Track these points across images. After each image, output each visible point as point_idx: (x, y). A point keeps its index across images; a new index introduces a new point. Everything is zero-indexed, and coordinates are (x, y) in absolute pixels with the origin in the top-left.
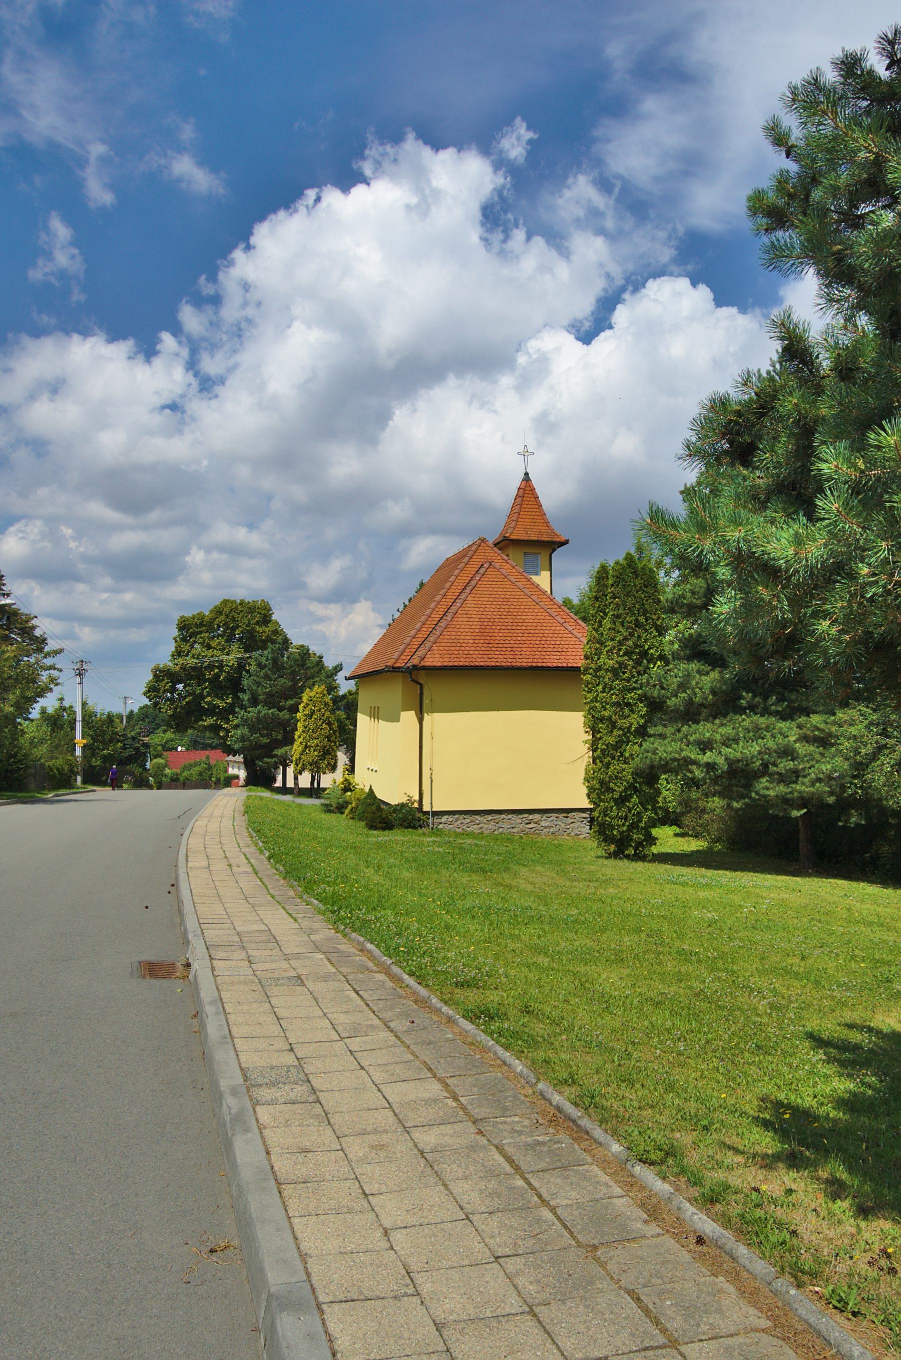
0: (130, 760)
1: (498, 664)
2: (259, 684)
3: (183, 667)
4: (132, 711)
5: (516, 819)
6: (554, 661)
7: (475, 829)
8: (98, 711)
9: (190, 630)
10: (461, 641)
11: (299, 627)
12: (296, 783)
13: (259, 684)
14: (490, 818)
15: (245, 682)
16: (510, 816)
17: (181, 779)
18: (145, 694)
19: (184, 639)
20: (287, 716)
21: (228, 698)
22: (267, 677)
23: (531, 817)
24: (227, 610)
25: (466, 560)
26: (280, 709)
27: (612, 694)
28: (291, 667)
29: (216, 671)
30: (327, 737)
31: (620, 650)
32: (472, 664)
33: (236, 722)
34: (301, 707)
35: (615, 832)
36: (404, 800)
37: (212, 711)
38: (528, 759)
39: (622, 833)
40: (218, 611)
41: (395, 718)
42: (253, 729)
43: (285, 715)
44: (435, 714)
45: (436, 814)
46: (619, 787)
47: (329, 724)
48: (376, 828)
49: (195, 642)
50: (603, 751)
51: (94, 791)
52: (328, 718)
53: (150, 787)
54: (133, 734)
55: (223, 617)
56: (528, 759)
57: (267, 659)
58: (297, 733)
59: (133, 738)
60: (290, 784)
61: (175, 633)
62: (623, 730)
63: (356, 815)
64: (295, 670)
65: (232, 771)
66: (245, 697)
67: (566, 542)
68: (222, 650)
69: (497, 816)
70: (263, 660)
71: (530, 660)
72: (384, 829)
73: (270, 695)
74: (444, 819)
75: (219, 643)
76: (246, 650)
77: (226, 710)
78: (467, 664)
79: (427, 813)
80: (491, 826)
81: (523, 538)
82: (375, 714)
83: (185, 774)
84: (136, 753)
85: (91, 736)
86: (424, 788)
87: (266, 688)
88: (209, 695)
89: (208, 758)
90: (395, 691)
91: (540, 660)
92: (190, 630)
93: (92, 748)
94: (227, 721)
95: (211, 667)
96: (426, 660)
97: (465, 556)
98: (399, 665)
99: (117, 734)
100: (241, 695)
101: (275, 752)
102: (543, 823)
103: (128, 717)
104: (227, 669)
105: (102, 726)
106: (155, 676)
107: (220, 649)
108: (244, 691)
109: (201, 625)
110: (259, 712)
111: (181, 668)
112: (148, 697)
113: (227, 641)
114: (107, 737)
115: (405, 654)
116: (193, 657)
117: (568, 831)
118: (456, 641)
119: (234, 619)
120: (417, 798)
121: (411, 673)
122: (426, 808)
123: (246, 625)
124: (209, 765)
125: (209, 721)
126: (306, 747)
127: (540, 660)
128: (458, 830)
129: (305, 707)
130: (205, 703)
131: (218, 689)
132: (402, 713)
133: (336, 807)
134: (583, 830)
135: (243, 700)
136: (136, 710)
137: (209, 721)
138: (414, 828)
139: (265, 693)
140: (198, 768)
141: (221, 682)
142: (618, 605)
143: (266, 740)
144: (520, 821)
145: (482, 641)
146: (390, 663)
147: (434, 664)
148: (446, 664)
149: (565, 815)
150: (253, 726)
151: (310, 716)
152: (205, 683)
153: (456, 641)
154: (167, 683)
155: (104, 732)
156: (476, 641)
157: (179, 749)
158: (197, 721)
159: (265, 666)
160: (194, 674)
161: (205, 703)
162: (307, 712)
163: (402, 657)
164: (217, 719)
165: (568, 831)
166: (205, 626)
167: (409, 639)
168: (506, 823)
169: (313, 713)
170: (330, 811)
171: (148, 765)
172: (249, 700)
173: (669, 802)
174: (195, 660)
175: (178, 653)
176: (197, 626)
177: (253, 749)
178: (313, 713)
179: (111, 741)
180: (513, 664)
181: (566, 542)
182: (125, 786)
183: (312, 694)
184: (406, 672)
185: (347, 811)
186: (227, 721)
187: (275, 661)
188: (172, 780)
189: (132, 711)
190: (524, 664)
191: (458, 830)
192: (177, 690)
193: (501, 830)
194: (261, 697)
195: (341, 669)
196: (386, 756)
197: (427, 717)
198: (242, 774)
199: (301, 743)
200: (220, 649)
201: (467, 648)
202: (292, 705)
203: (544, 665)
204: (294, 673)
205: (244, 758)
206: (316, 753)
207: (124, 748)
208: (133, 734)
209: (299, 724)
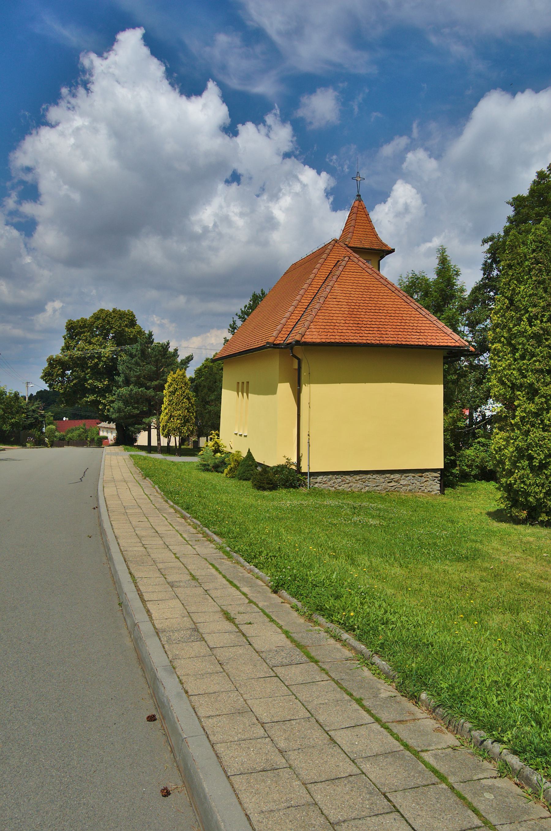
0: (31, 426)
1: (369, 342)
2: (131, 369)
3: (71, 358)
4: (32, 395)
5: (380, 478)
6: (414, 340)
7: (345, 487)
8: (8, 391)
9: (74, 330)
10: (335, 321)
11: (158, 328)
12: (159, 444)
13: (131, 369)
14: (358, 478)
15: (120, 368)
16: (374, 476)
17: (67, 439)
18: (42, 378)
19: (71, 338)
20: (153, 394)
21: (105, 381)
22: (137, 364)
23: (392, 477)
24: (103, 315)
25: (324, 256)
26: (148, 388)
27: (535, 361)
28: (156, 356)
29: (96, 360)
30: (187, 409)
31: (543, 316)
32: (347, 341)
33: (111, 398)
34: (166, 386)
35: (531, 499)
36: (283, 462)
37: (93, 390)
38: (395, 425)
39: (538, 500)
40: (96, 317)
41: (273, 391)
42: (126, 403)
43: (151, 392)
44: (311, 385)
45: (313, 474)
46: (539, 454)
47: (188, 399)
48: (264, 489)
49: (80, 339)
50: (522, 418)
51: (4, 450)
52: (187, 394)
53: (45, 445)
54: (33, 408)
55: (100, 321)
56: (395, 425)
57: (137, 351)
58: (163, 406)
59: (34, 411)
60: (154, 443)
61: (65, 332)
62: (545, 397)
63: (232, 474)
64: (158, 359)
65: (102, 434)
66: (120, 379)
67: (393, 251)
68: (100, 345)
69: (364, 476)
70: (134, 351)
71: (396, 339)
72: (271, 489)
73: (138, 377)
74: (319, 479)
75: (98, 340)
76: (118, 345)
77: (103, 390)
78: (342, 341)
79: (305, 474)
80: (359, 485)
81: (358, 246)
82: (244, 388)
83: (69, 435)
84: (36, 421)
85: (2, 409)
86: (301, 452)
87: (136, 372)
88: (90, 378)
89: (84, 425)
90: (273, 365)
91: (403, 339)
92: (74, 330)
93: (3, 418)
94: (105, 397)
95: (92, 357)
96: (305, 336)
97: (323, 253)
98: (278, 342)
99: (21, 407)
100: (116, 378)
101: (144, 420)
102: (402, 482)
103: (29, 398)
104: (104, 359)
105: (10, 402)
106: (50, 364)
107: (98, 345)
108: (118, 375)
109: (84, 326)
110: (132, 390)
111: (70, 358)
112: (45, 380)
113: (103, 338)
114: (14, 410)
115: (282, 332)
116: (78, 350)
117: (423, 488)
118: (330, 321)
119: (109, 323)
120: (295, 460)
121: (292, 349)
122: (304, 469)
123: (119, 327)
124: (85, 429)
125: (91, 398)
126: (171, 416)
127: (403, 339)
128: (331, 489)
129: (169, 386)
130: (88, 384)
131: (97, 373)
132: (279, 384)
133: (213, 467)
134: (434, 487)
135: (119, 381)
136: (35, 394)
137: (91, 398)
138: (294, 487)
139: (135, 376)
140: (78, 432)
141: (100, 369)
142: (540, 270)
143: (136, 412)
144: (382, 480)
145: (352, 322)
146: (271, 340)
147: (314, 340)
148: (324, 341)
149: (420, 474)
150: (127, 401)
151: (173, 393)
152: (87, 369)
153: (330, 321)
154: (59, 369)
155: (12, 407)
156: (347, 322)
157: (64, 419)
158: (81, 398)
159: (136, 355)
160: (80, 363)
161: (88, 384)
162: (171, 389)
163: (280, 335)
164: (97, 396)
165: (423, 488)
166: (87, 327)
167: (284, 320)
168: (373, 483)
169: (176, 390)
170: (208, 470)
171: (44, 430)
172: (123, 381)
173: (487, 462)
174: (80, 352)
175: (67, 347)
176: (81, 327)
177: (127, 418)
178: (176, 390)
179: (17, 412)
180: (382, 342)
181: (393, 251)
182: (28, 445)
183: (175, 376)
184: (285, 348)
185: (226, 471)
186: (105, 397)
187: (143, 352)
188: (60, 439)
189: (32, 395)
190: (391, 342)
191: (331, 489)
192: (67, 375)
193: (367, 488)
194: (133, 379)
195: (192, 359)
196: (254, 423)
197: (305, 389)
198: (111, 436)
199: (167, 414)
200: (98, 345)
201: (340, 328)
202: (156, 385)
203: (408, 343)
204: (157, 361)
205: (116, 425)
206: (178, 421)
207: (27, 418)
208: (33, 408)
209: (165, 399)
